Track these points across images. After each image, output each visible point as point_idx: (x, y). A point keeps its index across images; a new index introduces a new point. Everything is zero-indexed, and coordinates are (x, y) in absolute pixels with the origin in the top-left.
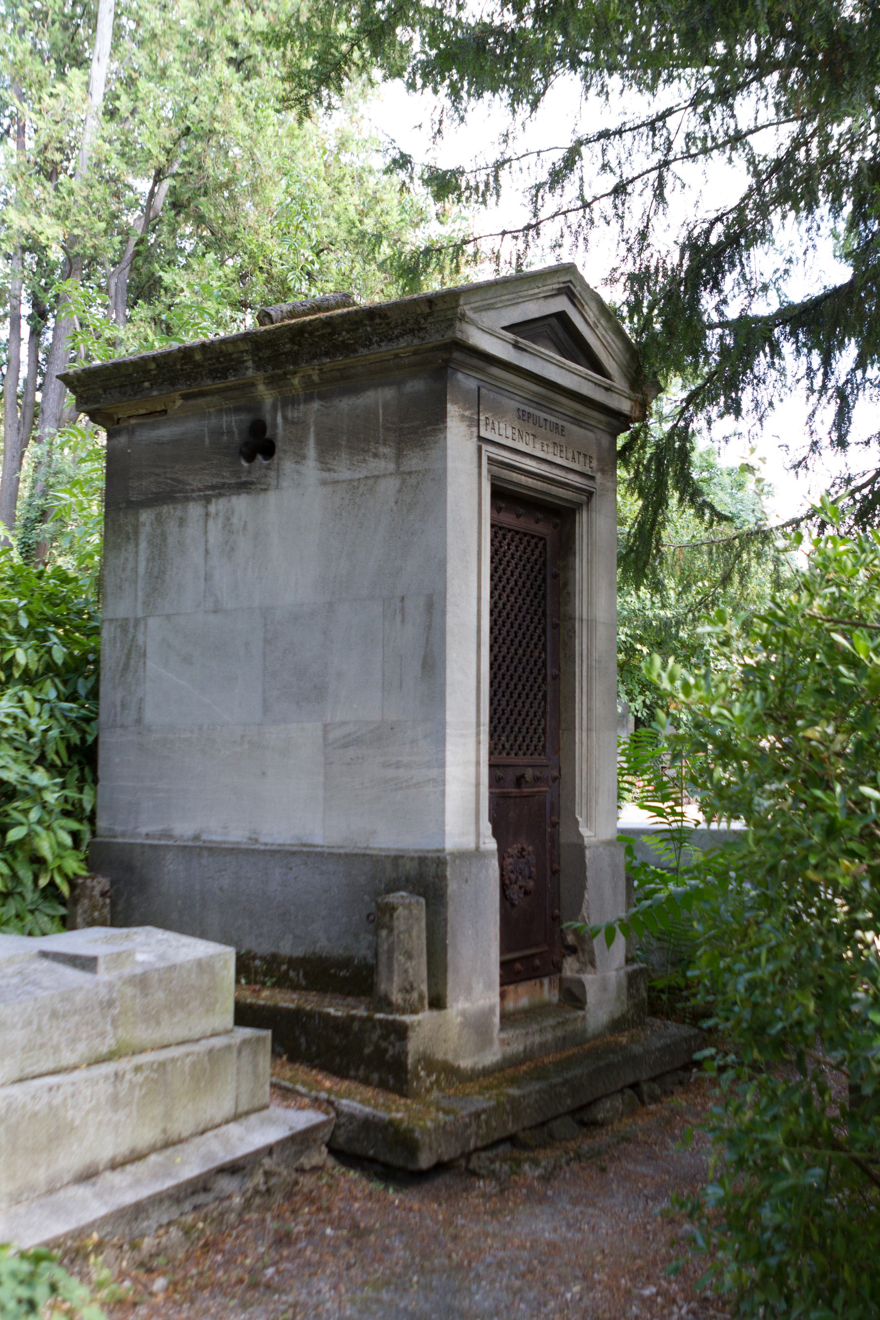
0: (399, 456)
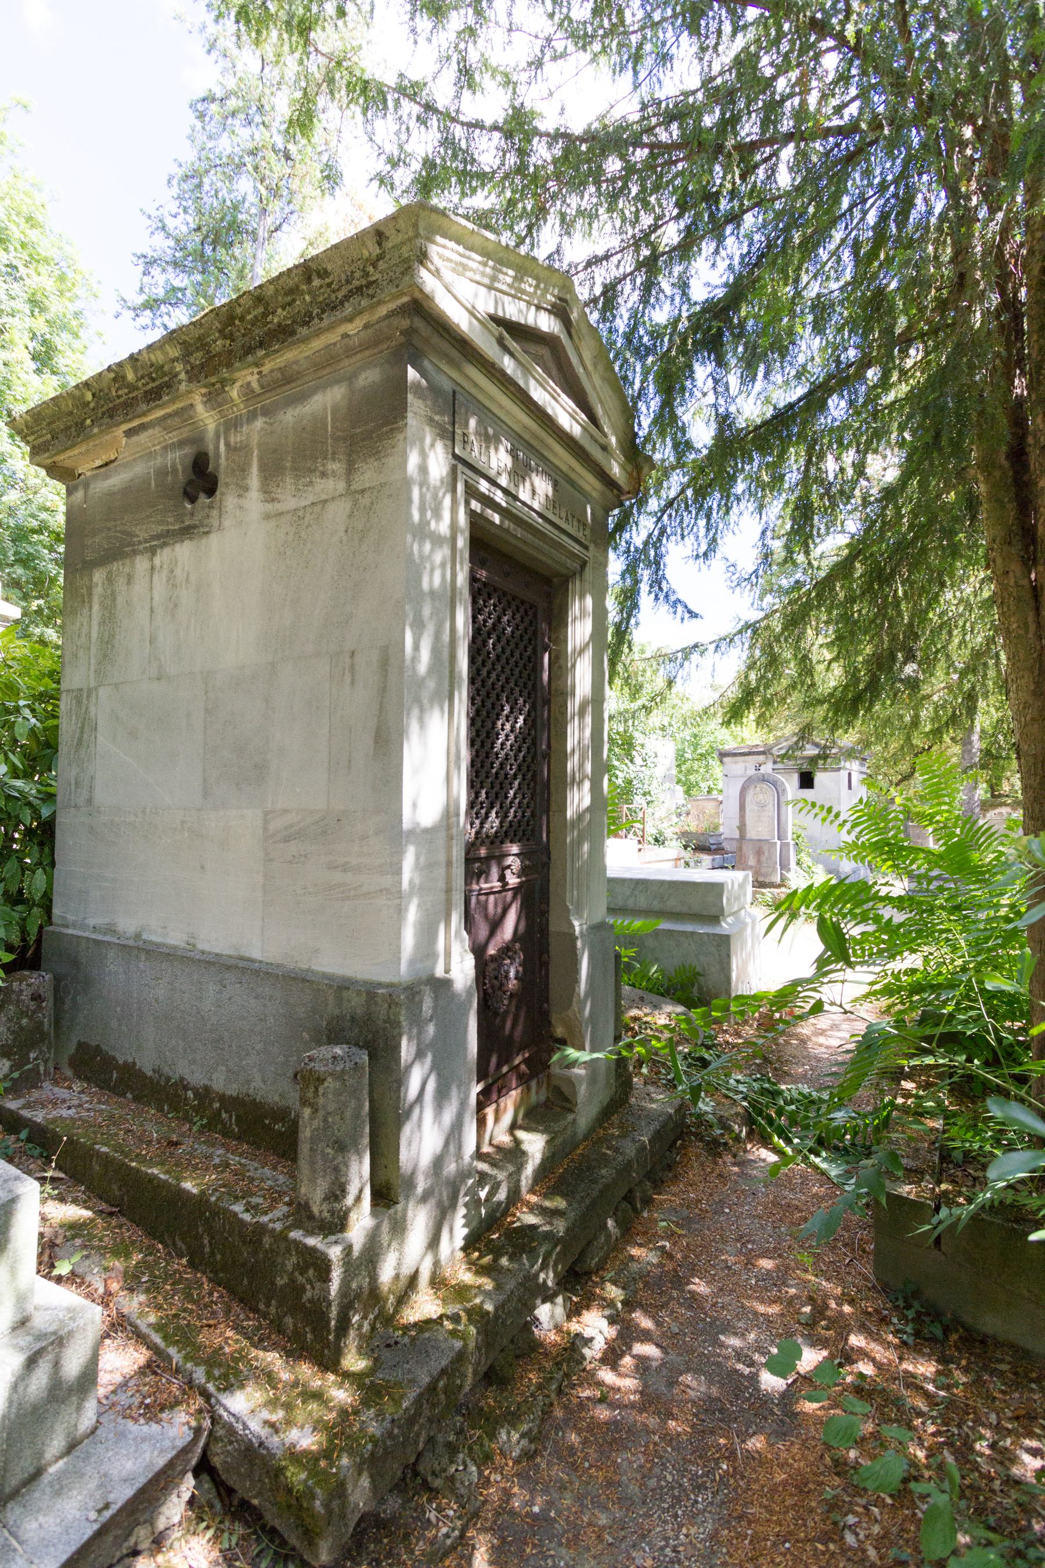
0: (350, 470)
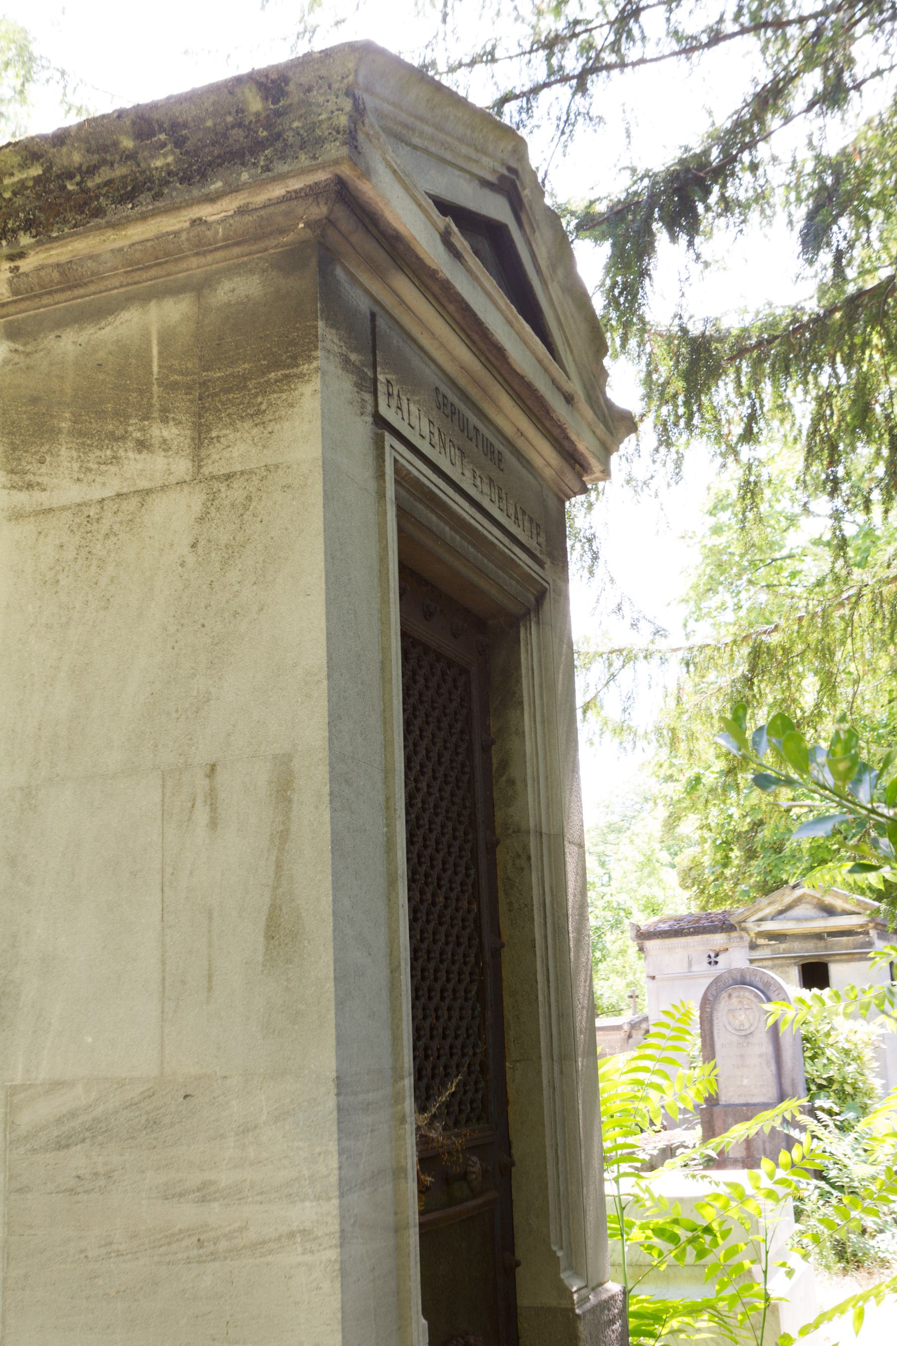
0: (201, 439)
